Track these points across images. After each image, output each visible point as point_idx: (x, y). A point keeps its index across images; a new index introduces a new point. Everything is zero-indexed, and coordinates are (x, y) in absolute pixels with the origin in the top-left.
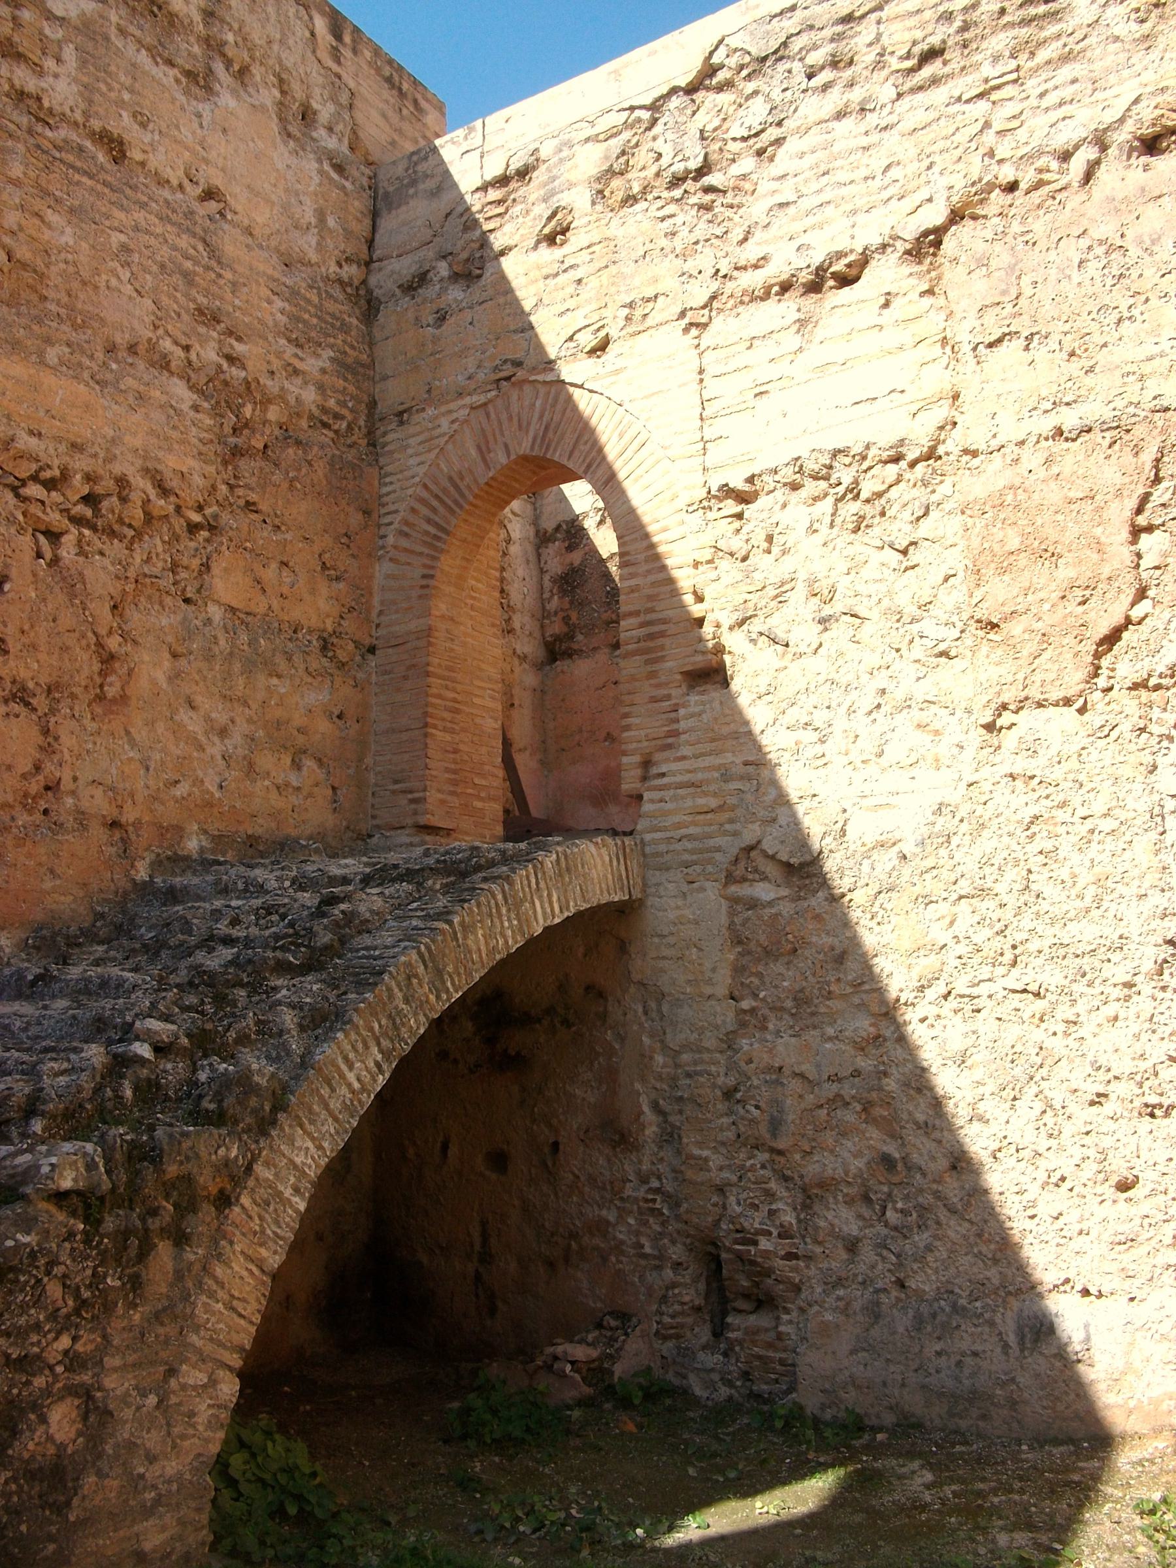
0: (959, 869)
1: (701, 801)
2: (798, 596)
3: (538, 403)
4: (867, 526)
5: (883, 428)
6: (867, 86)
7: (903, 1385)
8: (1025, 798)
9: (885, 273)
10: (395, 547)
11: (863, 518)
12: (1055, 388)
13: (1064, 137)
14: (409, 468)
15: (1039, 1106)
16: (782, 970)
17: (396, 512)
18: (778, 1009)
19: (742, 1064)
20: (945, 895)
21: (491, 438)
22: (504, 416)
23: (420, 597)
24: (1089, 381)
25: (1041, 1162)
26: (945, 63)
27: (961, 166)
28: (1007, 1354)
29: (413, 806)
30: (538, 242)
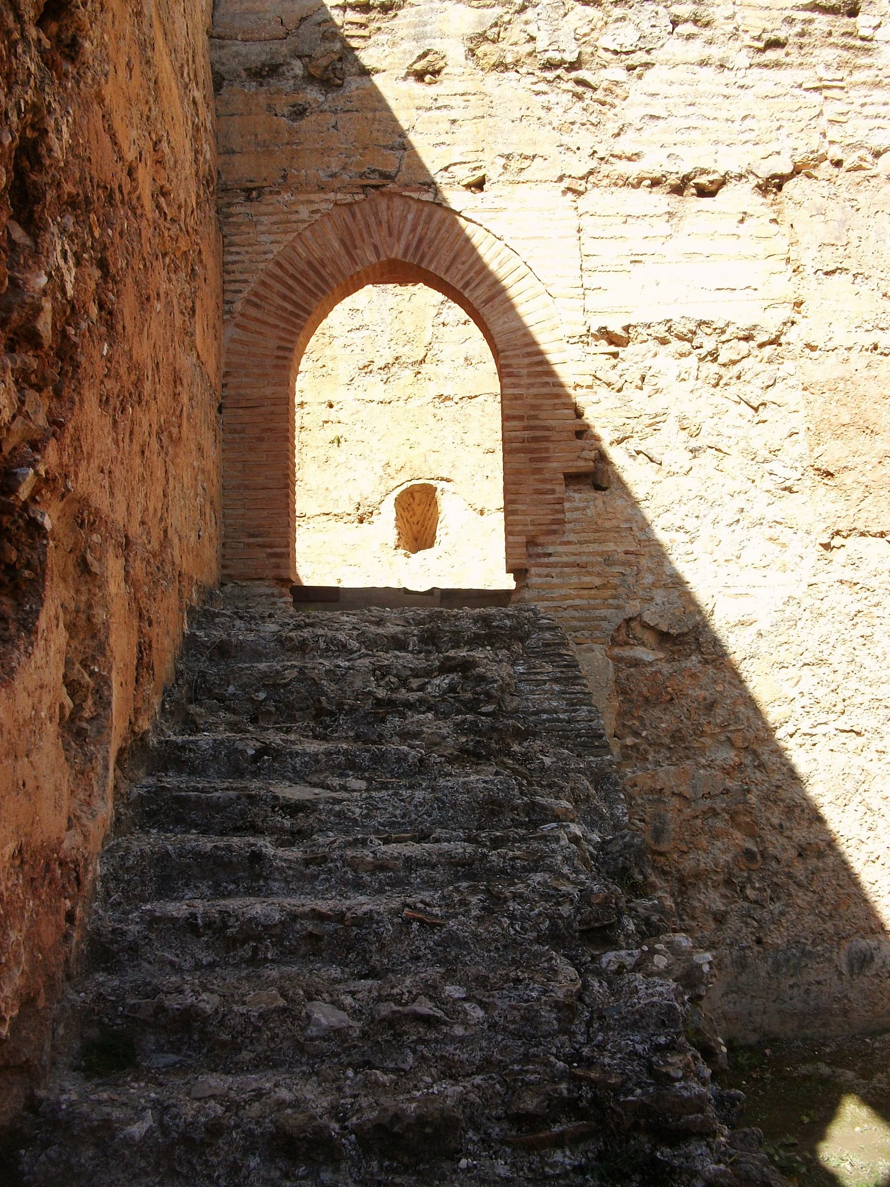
0: (804, 644)
1: (587, 579)
2: (670, 427)
3: (410, 217)
4: (726, 384)
5: (741, 313)
6: (723, 49)
7: (765, 1013)
8: (851, 598)
9: (738, 197)
10: (242, 315)
11: (721, 377)
12: (874, 316)
14: (259, 243)
15: (862, 809)
16: (660, 714)
17: (245, 281)
18: (656, 744)
19: (628, 788)
20: (794, 662)
21: (357, 236)
22: (372, 220)
23: (276, 366)
25: (863, 847)
26: (787, 55)
27: (802, 135)
28: (841, 979)
29: (274, 560)
30: (408, 74)
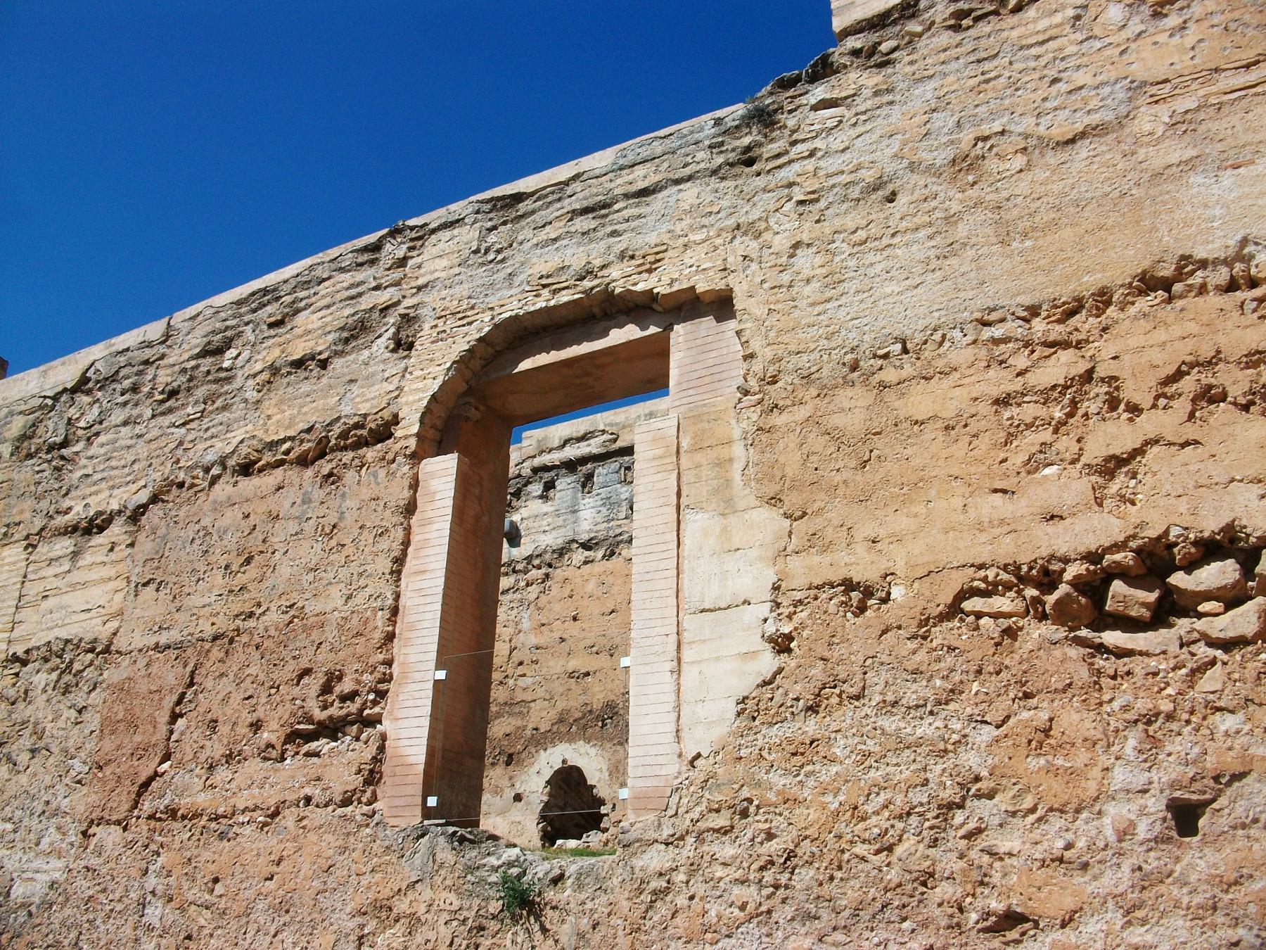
13: (210, 457)
24: (177, 616)
